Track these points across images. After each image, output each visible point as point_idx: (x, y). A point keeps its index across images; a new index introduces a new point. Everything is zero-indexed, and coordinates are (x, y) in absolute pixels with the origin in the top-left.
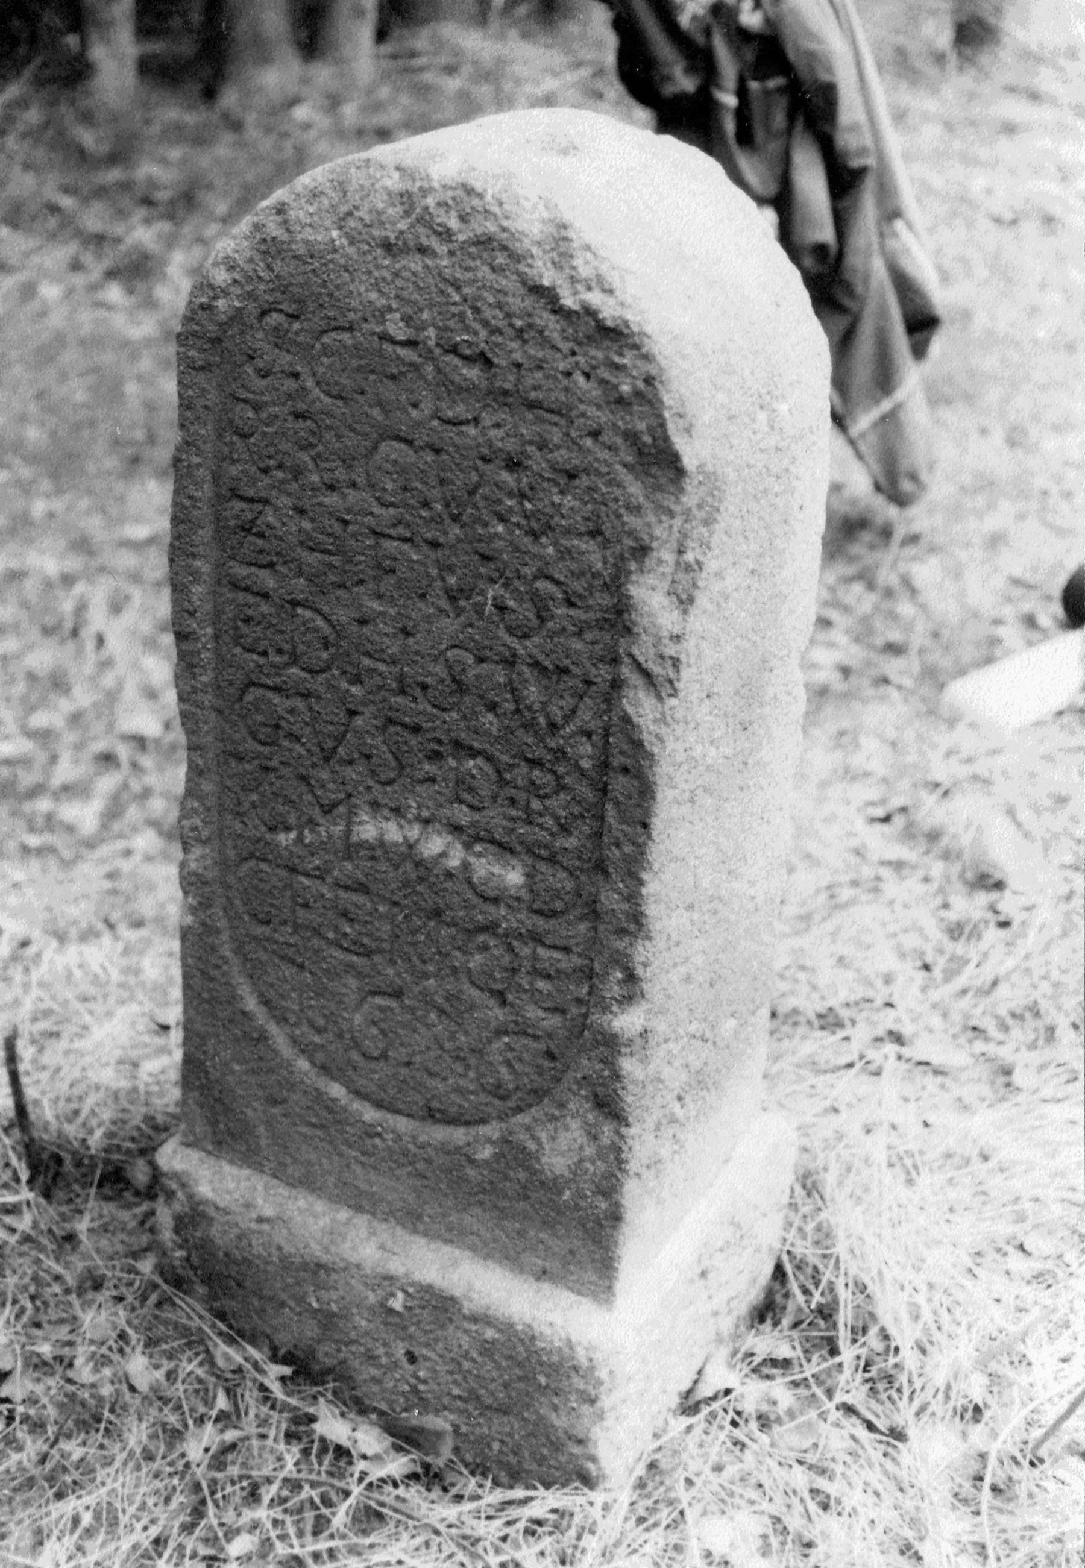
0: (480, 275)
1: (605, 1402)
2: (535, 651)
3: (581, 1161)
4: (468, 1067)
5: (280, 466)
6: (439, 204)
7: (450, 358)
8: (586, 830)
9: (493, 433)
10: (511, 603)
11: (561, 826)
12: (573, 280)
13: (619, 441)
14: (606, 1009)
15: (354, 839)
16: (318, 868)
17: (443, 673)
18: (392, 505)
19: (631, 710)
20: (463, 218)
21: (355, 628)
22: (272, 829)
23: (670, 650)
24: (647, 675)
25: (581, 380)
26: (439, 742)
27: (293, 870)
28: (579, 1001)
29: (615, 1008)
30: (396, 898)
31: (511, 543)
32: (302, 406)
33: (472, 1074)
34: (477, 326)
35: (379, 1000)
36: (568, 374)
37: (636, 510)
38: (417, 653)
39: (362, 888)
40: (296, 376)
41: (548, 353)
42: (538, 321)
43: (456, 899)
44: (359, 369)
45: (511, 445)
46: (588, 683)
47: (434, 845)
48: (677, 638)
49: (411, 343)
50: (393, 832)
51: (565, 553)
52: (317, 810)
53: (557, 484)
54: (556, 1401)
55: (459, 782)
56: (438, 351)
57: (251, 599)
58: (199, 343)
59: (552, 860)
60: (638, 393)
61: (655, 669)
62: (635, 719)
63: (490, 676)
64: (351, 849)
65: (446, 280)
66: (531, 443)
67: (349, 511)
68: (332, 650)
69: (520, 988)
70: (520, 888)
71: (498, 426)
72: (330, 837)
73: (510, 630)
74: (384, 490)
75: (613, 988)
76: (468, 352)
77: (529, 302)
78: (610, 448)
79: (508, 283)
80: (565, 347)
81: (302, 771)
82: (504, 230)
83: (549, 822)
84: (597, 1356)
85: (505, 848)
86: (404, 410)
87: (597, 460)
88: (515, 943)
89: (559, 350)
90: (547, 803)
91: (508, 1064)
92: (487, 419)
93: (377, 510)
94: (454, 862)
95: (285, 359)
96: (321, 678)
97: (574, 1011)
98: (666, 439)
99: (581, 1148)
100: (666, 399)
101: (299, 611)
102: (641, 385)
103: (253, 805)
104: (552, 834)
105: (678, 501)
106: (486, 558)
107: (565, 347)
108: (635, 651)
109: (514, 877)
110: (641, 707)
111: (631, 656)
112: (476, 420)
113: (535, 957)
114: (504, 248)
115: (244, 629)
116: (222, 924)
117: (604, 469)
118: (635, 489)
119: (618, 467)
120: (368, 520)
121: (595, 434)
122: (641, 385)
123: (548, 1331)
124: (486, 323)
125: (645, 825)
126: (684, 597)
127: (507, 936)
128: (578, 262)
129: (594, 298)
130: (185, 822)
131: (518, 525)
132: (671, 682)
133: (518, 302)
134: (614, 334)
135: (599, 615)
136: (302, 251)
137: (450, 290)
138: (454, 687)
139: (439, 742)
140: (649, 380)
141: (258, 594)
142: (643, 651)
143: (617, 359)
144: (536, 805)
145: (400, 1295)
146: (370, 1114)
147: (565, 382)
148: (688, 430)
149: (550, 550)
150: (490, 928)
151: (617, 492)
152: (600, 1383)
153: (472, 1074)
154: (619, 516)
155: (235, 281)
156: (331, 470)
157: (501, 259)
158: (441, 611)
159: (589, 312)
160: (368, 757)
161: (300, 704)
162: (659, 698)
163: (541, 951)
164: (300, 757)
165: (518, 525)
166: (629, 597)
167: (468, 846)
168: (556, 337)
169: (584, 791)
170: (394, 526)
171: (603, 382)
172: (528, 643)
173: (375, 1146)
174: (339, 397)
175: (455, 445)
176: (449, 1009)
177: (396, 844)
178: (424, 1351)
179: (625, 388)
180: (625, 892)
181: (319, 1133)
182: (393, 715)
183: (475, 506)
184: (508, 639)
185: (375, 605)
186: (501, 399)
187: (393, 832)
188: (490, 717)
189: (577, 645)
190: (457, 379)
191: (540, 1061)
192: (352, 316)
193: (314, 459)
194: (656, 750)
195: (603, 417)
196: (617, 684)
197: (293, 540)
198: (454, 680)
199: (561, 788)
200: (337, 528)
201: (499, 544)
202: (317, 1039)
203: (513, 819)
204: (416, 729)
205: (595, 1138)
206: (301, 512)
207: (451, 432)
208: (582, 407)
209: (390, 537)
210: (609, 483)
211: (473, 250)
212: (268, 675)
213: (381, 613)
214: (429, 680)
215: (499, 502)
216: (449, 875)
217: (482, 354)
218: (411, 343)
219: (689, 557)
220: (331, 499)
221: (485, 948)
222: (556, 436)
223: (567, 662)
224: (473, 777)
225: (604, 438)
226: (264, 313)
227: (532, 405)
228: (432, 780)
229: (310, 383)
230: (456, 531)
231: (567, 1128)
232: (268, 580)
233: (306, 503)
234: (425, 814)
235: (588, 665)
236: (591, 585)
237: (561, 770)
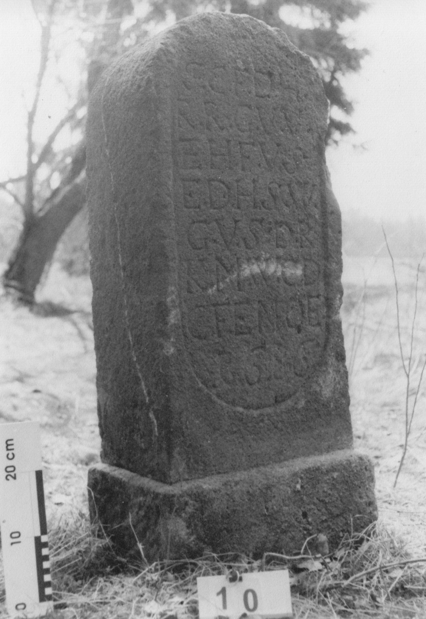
3: (336, 384)
7: (258, 74)
15: (242, 277)
47: (272, 268)
50: (256, 269)
64: (240, 284)
72: (231, 281)
79: (274, 47)
85: (295, 261)
99: (335, 379)
101: (213, 183)
167: (283, 265)
177: (258, 274)
184: (289, 175)
192: (224, 61)
199: (310, 229)
209: (247, 144)
216: (278, 279)
231: (329, 373)
232: (199, 173)
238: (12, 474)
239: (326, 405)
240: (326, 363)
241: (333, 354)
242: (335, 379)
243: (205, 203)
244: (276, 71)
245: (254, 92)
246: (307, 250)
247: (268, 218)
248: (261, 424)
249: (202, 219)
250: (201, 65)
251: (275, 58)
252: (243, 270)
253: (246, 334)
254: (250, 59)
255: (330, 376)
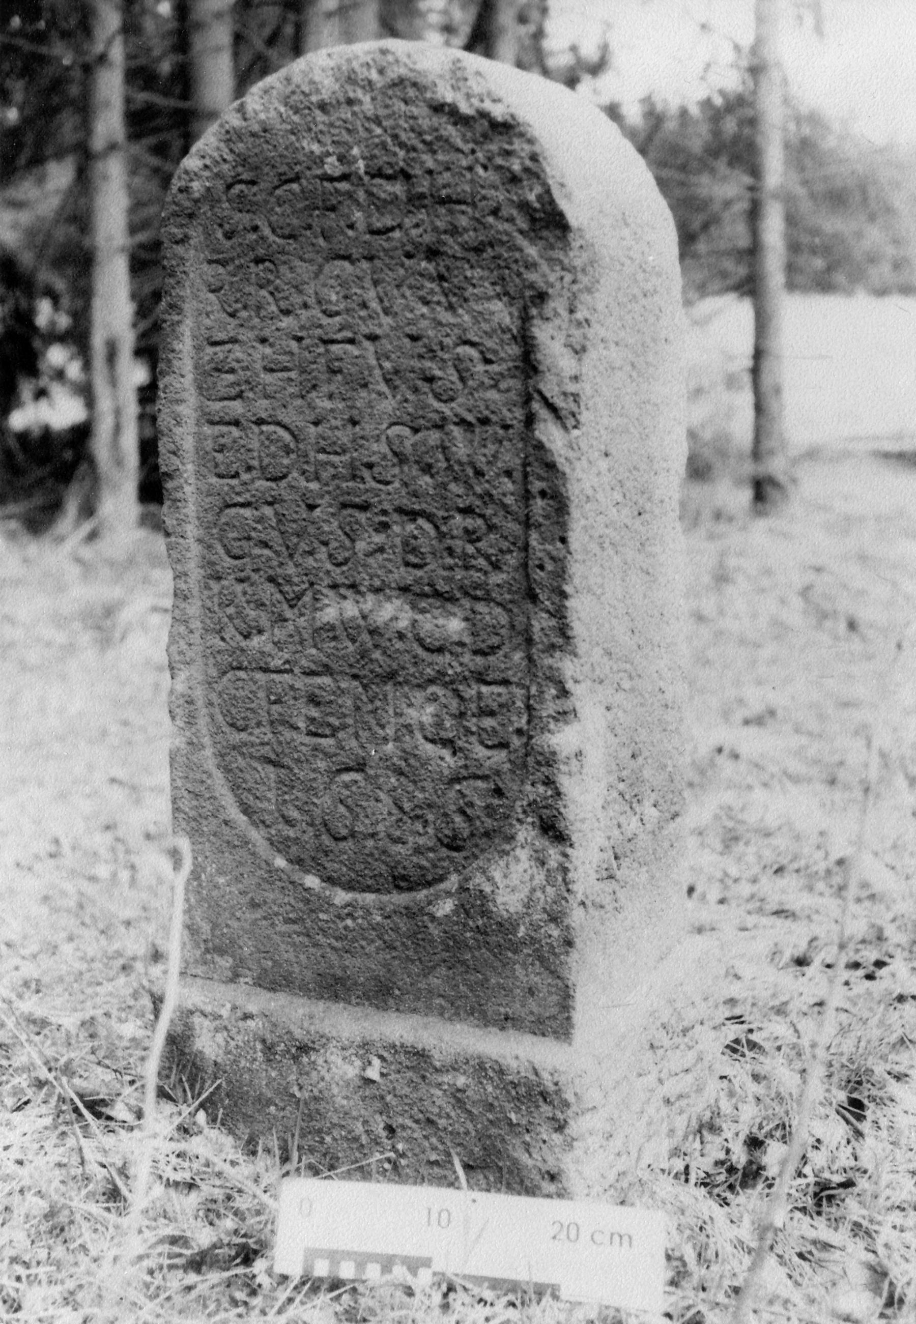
0: (396, 108)
1: (573, 1128)
2: (460, 410)
3: (533, 890)
4: (426, 823)
5: (245, 307)
6: (362, 65)
7: (378, 181)
8: (513, 562)
9: (414, 232)
10: (438, 373)
11: (491, 563)
12: (468, 96)
13: (515, 212)
14: (545, 729)
16: (287, 662)
17: (384, 449)
18: (337, 313)
19: (544, 439)
20: (381, 72)
21: (312, 429)
22: (247, 636)
23: (571, 388)
24: (553, 409)
25: (481, 171)
26: (384, 512)
27: (266, 670)
28: (519, 732)
29: (552, 726)
30: (355, 671)
31: (434, 319)
32: (261, 252)
33: (430, 830)
34: (397, 149)
35: (347, 777)
36: (470, 169)
37: (531, 266)
38: (362, 438)
39: (327, 670)
40: (255, 229)
41: (453, 156)
42: (444, 133)
43: (407, 657)
44: (306, 208)
45: (428, 239)
46: (506, 427)
48: (576, 378)
49: (345, 177)
50: (350, 609)
51: (478, 317)
52: (285, 606)
53: (468, 261)
54: (527, 1138)
55: (406, 544)
56: (366, 179)
57: (225, 429)
58: (178, 220)
59: (487, 599)
60: (526, 170)
61: (559, 402)
62: (548, 445)
63: (424, 442)
65: (368, 119)
66: (445, 232)
67: (302, 328)
68: (293, 456)
69: (468, 732)
70: (460, 633)
71: (417, 226)
73: (438, 397)
74: (330, 302)
75: (549, 708)
76: (390, 172)
77: (436, 120)
78: (507, 220)
79: (420, 111)
80: (467, 148)
81: (271, 572)
82: (411, 70)
83: (481, 562)
84: (562, 1080)
86: (342, 232)
87: (498, 232)
88: (461, 688)
89: (462, 152)
90: (479, 545)
91: (462, 812)
92: (408, 222)
93: (325, 321)
94: (403, 624)
95: (245, 219)
96: (283, 483)
97: (516, 742)
98: (552, 202)
99: (532, 878)
100: (548, 169)
102: (528, 163)
103: (230, 617)
104: (486, 573)
105: (567, 255)
106: (414, 338)
107: (467, 148)
108: (541, 386)
109: (455, 626)
110: (550, 433)
111: (540, 393)
112: (400, 226)
113: (480, 696)
114: (415, 85)
115: (219, 457)
116: (207, 741)
117: (505, 238)
118: (532, 251)
119: (515, 234)
120: (319, 331)
121: (495, 212)
122: (528, 163)
123: (514, 1064)
124: (402, 145)
125: (563, 540)
126: (578, 347)
127: (452, 682)
128: (472, 82)
129: (488, 106)
130: (174, 648)
131: (439, 303)
132: (574, 415)
133: (426, 122)
134: (505, 128)
135: (511, 364)
136: (256, 128)
137: (373, 126)
138: (395, 460)
139: (384, 512)
140: (534, 158)
141: (229, 423)
142: (550, 388)
143: (507, 147)
144: (470, 549)
145: (376, 1062)
146: (341, 897)
147: (468, 176)
148: (568, 196)
149: (466, 318)
150: (439, 678)
151: (517, 255)
152: (566, 1104)
153: (430, 830)
154: (519, 275)
155: (206, 166)
156: (287, 298)
157: (411, 93)
158: (380, 394)
159: (483, 115)
160: (325, 544)
161: (268, 511)
162: (565, 428)
163: (484, 689)
164: (269, 559)
165: (439, 303)
166: (534, 338)
168: (459, 143)
169: (513, 527)
170: (340, 330)
171: (499, 168)
172: (453, 405)
173: (346, 928)
174: (291, 236)
175: (384, 250)
176: (406, 769)
178: (400, 1120)
179: (516, 167)
180: (551, 608)
181: (296, 927)
182: (347, 498)
183: (403, 296)
184: (436, 404)
185: (328, 404)
186: (417, 203)
187: (350, 609)
188: (427, 479)
189: (492, 395)
190: (383, 195)
191: (490, 800)
192: (298, 168)
193: (272, 294)
194: (567, 470)
195: (501, 195)
196: (530, 420)
197: (258, 366)
198: (395, 454)
200: (294, 345)
201: (424, 324)
202: (291, 833)
203: (451, 568)
204: (364, 507)
205: (543, 863)
206: (263, 341)
207: (380, 241)
208: (483, 192)
210: (510, 249)
211: (390, 92)
212: (238, 494)
213: (332, 410)
214: (374, 459)
215: (422, 287)
216: (401, 636)
217: (402, 171)
218: (345, 177)
219: (579, 315)
220: (286, 322)
221: (434, 699)
222: (463, 221)
223: (486, 413)
224: (416, 538)
225: (504, 213)
226: (229, 187)
227: (443, 202)
228: (381, 550)
229: (267, 231)
230: (387, 321)
231: (517, 860)
233: (267, 333)
234: (377, 583)
235: (505, 411)
236: (502, 340)
237: (489, 512)
238: (563, 1235)
239: (506, 927)
240: (511, 838)
241: (530, 820)
242: (532, 878)
243: (249, 469)
244: (418, 166)
245: (361, 226)
246: (476, 575)
247: (380, 502)
248: (349, 922)
249: (240, 499)
250: (253, 183)
251: (420, 134)
252: (321, 609)
253: (326, 736)
254: (355, 151)
255: (521, 867)
